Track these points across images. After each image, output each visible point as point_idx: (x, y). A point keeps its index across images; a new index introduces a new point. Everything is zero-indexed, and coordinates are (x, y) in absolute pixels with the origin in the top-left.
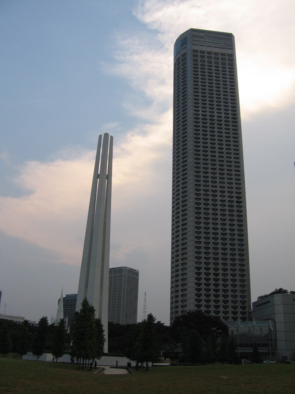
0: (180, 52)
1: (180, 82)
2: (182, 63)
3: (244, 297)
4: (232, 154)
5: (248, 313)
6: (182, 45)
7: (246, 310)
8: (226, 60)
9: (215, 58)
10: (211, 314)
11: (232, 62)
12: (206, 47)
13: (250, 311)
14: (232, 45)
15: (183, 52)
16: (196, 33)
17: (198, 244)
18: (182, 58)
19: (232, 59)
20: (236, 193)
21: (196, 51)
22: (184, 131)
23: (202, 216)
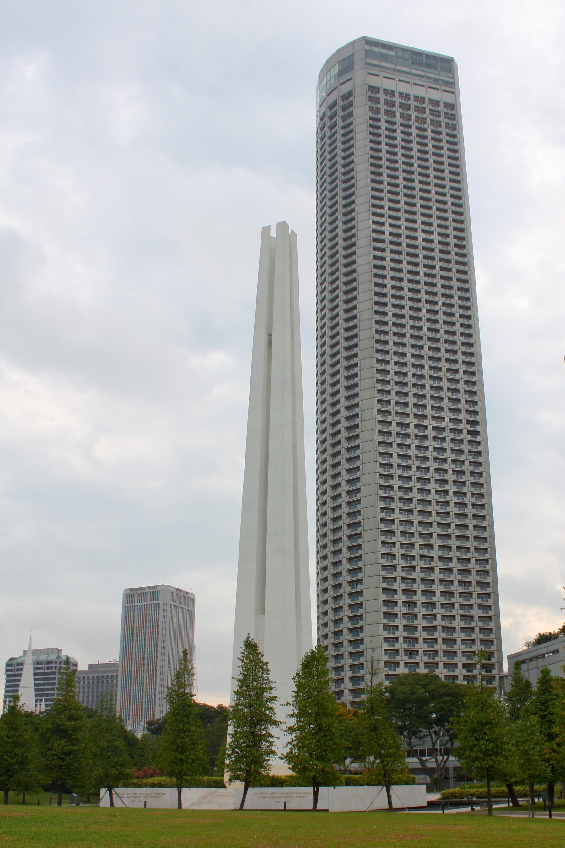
0: (336, 88)
1: (338, 149)
2: (342, 103)
3: (475, 433)
4: (458, 324)
5: (497, 678)
6: (341, 73)
7: (494, 672)
8: (440, 116)
9: (417, 109)
10: (418, 671)
11: (454, 122)
12: (398, 83)
13: (502, 674)
14: (454, 83)
15: (344, 89)
16: (376, 49)
17: (388, 549)
18: (341, 103)
19: (455, 125)
20: (469, 422)
21: (374, 89)
22: (350, 269)
23: (399, 574)
